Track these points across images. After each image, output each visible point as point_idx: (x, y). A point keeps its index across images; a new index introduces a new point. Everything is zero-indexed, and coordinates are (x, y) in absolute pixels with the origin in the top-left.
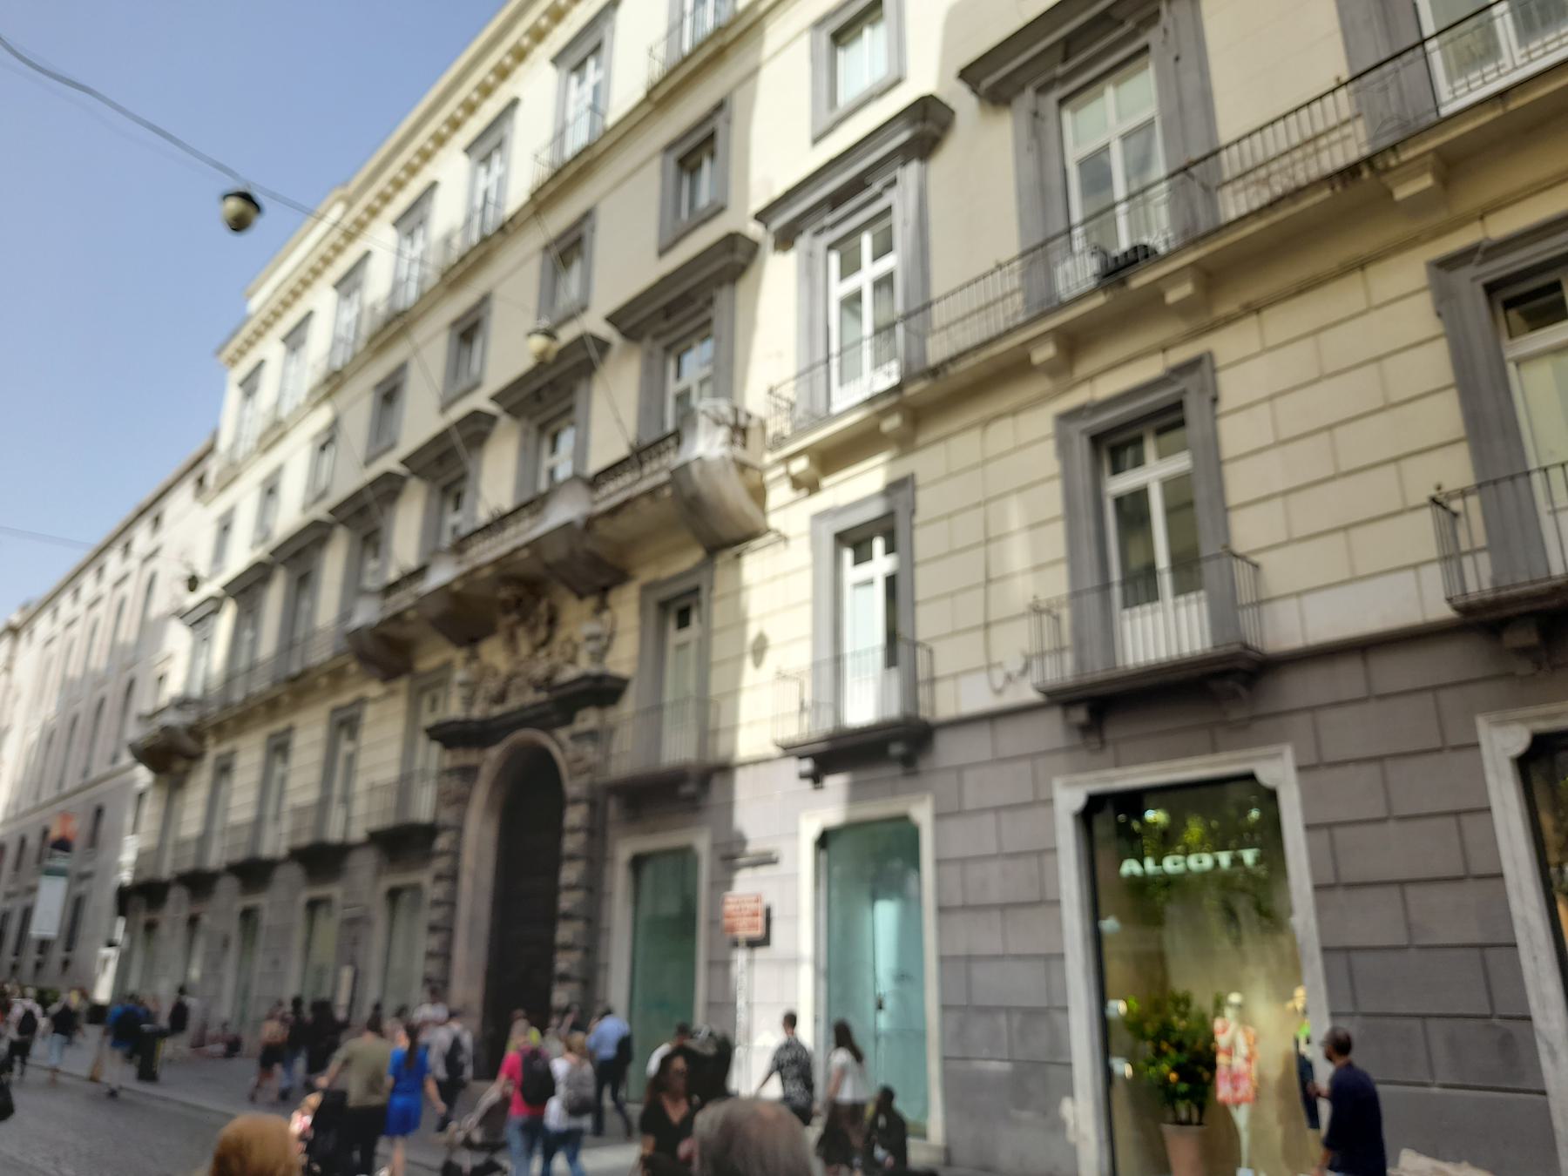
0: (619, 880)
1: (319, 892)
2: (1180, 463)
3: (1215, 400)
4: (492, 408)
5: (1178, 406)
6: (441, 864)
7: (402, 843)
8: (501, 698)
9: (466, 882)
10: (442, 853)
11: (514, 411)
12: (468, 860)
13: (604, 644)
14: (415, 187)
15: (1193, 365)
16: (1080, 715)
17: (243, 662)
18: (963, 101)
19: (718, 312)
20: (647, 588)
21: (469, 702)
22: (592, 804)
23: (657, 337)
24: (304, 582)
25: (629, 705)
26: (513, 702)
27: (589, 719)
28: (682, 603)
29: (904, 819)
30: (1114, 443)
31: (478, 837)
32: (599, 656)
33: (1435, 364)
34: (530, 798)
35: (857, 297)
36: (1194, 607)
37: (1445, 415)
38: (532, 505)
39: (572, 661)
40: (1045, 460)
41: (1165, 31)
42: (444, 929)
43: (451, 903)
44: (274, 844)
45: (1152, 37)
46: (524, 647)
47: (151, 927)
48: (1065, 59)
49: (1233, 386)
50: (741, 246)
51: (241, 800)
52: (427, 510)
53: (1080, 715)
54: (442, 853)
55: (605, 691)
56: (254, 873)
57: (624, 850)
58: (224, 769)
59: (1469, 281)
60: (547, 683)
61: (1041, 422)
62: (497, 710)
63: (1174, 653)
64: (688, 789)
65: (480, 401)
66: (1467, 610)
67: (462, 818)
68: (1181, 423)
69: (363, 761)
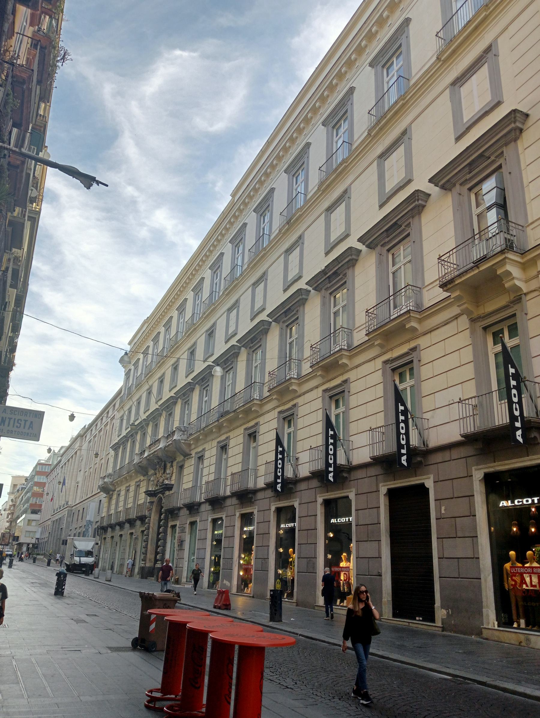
1: (193, 519)
3: (420, 361)
7: (142, 519)
9: (151, 530)
11: (446, 187)
12: (151, 525)
14: (238, 226)
15: (414, 349)
16: (480, 445)
17: (228, 395)
18: (433, 190)
19: (413, 230)
23: (327, 289)
24: (187, 403)
27: (167, 493)
28: (289, 418)
29: (423, 485)
33: (468, 354)
35: (257, 366)
36: (503, 405)
37: (469, 371)
38: (156, 442)
40: (378, 377)
41: (505, 159)
44: (200, 497)
47: (105, 538)
48: (470, 173)
49: (426, 356)
50: (421, 196)
51: (208, 473)
52: (281, 335)
53: (480, 445)
55: (169, 488)
56: (216, 502)
58: (201, 458)
61: (319, 392)
63: (381, 453)
64: (196, 507)
66: (465, 436)
67: (150, 514)
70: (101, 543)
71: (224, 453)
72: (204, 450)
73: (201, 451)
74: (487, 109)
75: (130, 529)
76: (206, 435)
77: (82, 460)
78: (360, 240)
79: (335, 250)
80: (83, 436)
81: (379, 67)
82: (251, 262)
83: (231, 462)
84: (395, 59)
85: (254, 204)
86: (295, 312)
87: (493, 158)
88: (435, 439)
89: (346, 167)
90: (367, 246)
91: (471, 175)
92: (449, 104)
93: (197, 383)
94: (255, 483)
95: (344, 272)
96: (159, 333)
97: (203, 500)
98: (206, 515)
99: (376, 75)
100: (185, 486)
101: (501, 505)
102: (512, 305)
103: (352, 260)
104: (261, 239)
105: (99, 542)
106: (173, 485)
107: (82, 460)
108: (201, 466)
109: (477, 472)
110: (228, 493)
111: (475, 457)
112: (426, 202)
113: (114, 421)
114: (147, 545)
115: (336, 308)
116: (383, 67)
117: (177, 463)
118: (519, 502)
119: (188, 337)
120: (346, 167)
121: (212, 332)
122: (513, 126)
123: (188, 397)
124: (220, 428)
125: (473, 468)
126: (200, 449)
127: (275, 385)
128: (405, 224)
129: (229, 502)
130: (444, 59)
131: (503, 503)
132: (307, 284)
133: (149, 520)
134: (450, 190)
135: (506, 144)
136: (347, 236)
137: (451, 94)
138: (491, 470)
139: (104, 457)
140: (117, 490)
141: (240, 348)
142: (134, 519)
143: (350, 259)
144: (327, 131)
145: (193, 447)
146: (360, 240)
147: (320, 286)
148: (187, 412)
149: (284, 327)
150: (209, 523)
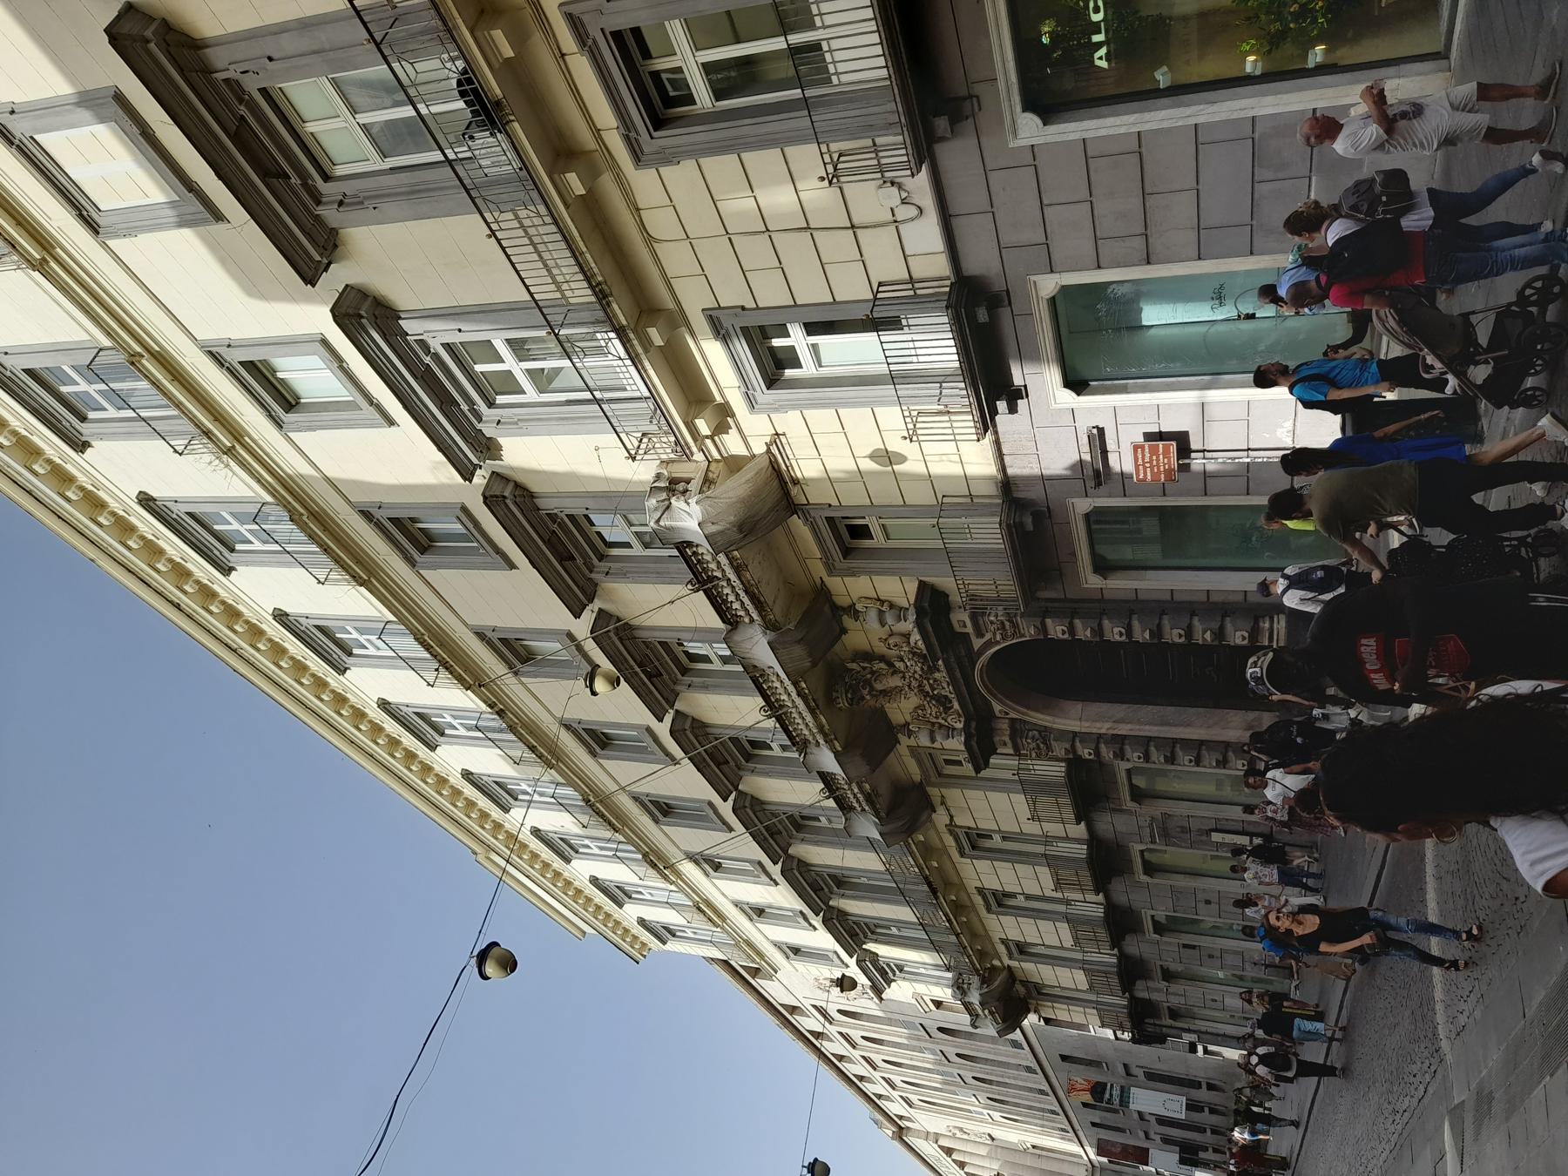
0: (1121, 584)
1: (1148, 925)
2: (677, 32)
4: (668, 718)
5: (617, 36)
6: (1107, 753)
7: (1087, 789)
8: (943, 702)
9: (1124, 729)
10: (1097, 752)
12: (1104, 728)
13: (886, 606)
18: (338, 277)
20: (831, 570)
21: (950, 731)
22: (1045, 614)
24: (842, 881)
25: (946, 582)
26: (948, 691)
27: (961, 619)
30: (660, 103)
31: (1075, 719)
32: (900, 613)
34: (1042, 672)
39: (907, 636)
40: (681, 175)
42: (1171, 748)
43: (1145, 743)
44: (1091, 905)
45: (252, 85)
46: (895, 681)
47: (1174, 1014)
52: (705, 688)
54: (1097, 752)
55: (932, 604)
57: (1093, 581)
58: (1022, 949)
59: (765, 396)
60: (928, 660)
61: (644, 182)
62: (956, 706)
65: (726, 808)
67: (1062, 735)
68: (636, 32)
69: (1010, 826)
70: (1189, 1031)
71: (867, 543)
72: (1003, 941)
73: (1008, 948)
74: (135, 130)
75: (1131, 871)
76: (974, 935)
77: (961, 1130)
78: (577, 615)
79: (496, 539)
80: (901, 1128)
81: (232, 557)
82: (610, 824)
83: (1052, 940)
84: (64, 389)
85: (557, 863)
86: (243, 110)
87: (243, 110)
88: (991, 469)
89: (312, 514)
90: (591, 600)
91: (576, 555)
92: (144, 238)
93: (785, 852)
94: (1078, 841)
95: (547, 519)
96: (642, 922)
97: (1101, 898)
98: (1142, 946)
99: (247, 564)
100: (1068, 941)
101: (1104, 64)
102: (590, 42)
103: (692, 728)
104: (490, 735)
105: (1188, 1038)
106: (923, 586)
107: (961, 1130)
108: (1020, 901)
109: (1021, 134)
110: (1080, 830)
111: (984, 140)
112: (151, 19)
113: (832, 1010)
114: (1187, 744)
115: (713, 657)
116: (83, 419)
117: (831, 570)
118: (1097, 10)
119: (624, 824)
120: (524, 726)
121: (591, 732)
122: (157, 49)
123: (821, 876)
124: (958, 908)
125: (1011, 145)
126: (1002, 949)
127: (542, 209)
128: (549, 523)
129: (1121, 898)
130: (233, 443)
131: (1100, 60)
132: (660, 720)
133: (1084, 737)
134: (334, 232)
135: (207, 71)
136: (570, 636)
137: (118, 236)
138: (1016, 99)
139: (937, 1048)
140: (1007, 962)
141: (741, 794)
142: (1119, 959)
143: (365, 315)
144: (355, 665)
145: (996, 963)
146: (577, 615)
147: (581, 583)
148: (894, 931)
149: (687, 679)
150: (1156, 881)
